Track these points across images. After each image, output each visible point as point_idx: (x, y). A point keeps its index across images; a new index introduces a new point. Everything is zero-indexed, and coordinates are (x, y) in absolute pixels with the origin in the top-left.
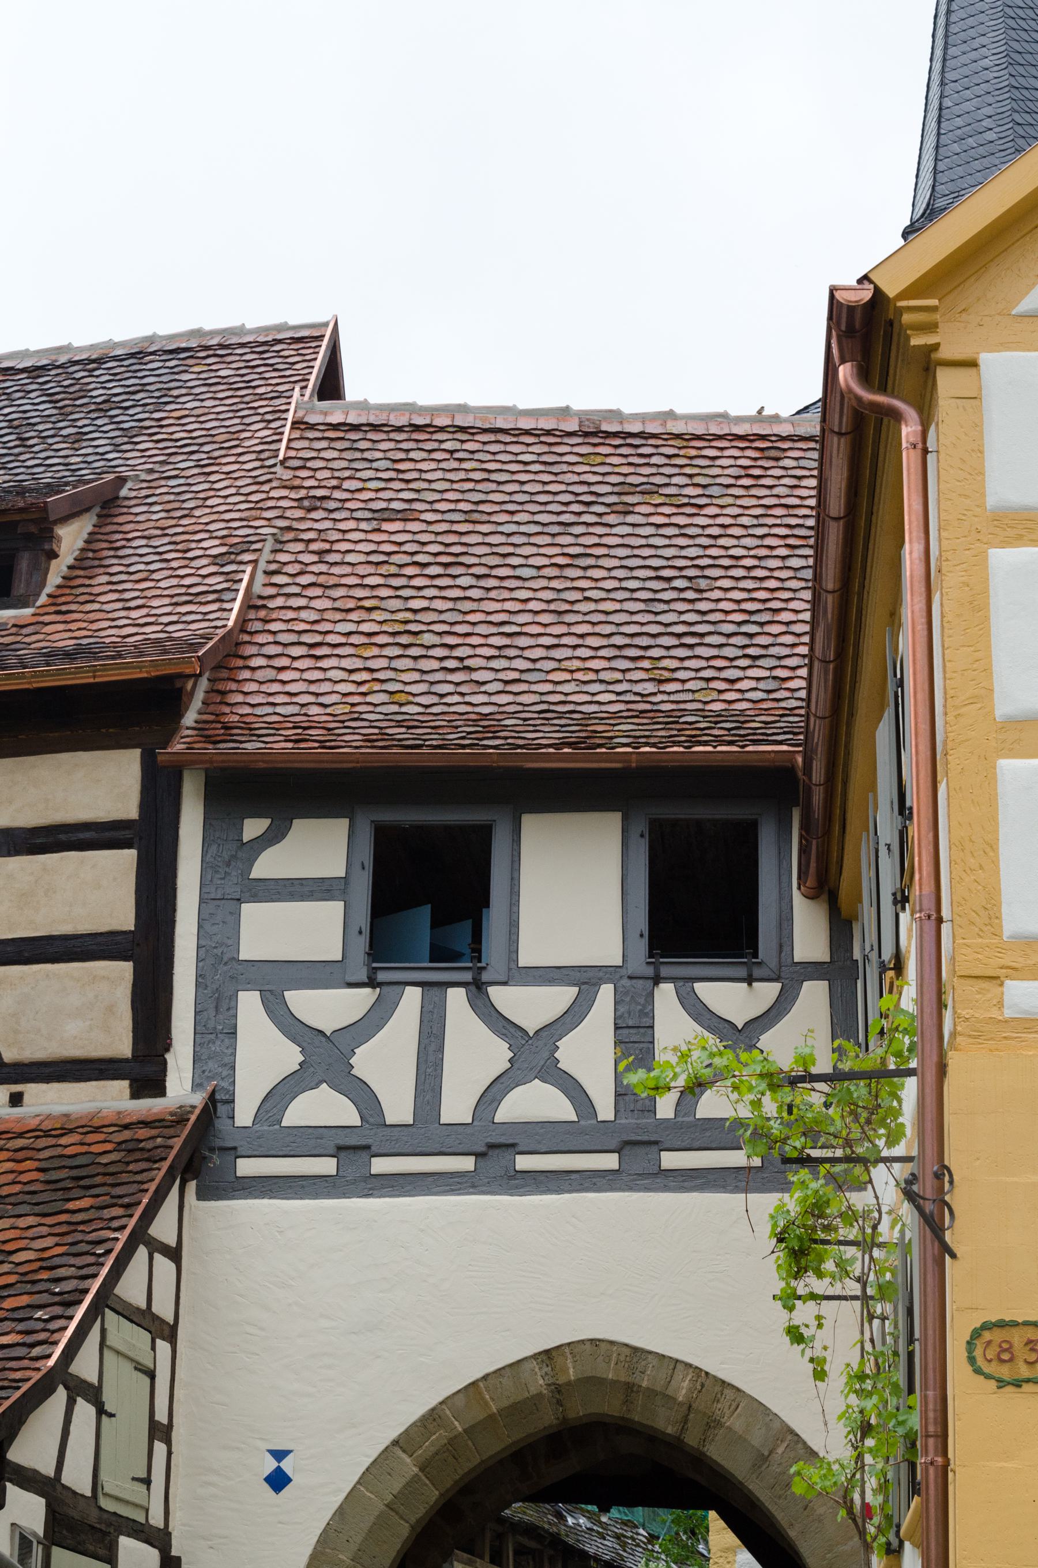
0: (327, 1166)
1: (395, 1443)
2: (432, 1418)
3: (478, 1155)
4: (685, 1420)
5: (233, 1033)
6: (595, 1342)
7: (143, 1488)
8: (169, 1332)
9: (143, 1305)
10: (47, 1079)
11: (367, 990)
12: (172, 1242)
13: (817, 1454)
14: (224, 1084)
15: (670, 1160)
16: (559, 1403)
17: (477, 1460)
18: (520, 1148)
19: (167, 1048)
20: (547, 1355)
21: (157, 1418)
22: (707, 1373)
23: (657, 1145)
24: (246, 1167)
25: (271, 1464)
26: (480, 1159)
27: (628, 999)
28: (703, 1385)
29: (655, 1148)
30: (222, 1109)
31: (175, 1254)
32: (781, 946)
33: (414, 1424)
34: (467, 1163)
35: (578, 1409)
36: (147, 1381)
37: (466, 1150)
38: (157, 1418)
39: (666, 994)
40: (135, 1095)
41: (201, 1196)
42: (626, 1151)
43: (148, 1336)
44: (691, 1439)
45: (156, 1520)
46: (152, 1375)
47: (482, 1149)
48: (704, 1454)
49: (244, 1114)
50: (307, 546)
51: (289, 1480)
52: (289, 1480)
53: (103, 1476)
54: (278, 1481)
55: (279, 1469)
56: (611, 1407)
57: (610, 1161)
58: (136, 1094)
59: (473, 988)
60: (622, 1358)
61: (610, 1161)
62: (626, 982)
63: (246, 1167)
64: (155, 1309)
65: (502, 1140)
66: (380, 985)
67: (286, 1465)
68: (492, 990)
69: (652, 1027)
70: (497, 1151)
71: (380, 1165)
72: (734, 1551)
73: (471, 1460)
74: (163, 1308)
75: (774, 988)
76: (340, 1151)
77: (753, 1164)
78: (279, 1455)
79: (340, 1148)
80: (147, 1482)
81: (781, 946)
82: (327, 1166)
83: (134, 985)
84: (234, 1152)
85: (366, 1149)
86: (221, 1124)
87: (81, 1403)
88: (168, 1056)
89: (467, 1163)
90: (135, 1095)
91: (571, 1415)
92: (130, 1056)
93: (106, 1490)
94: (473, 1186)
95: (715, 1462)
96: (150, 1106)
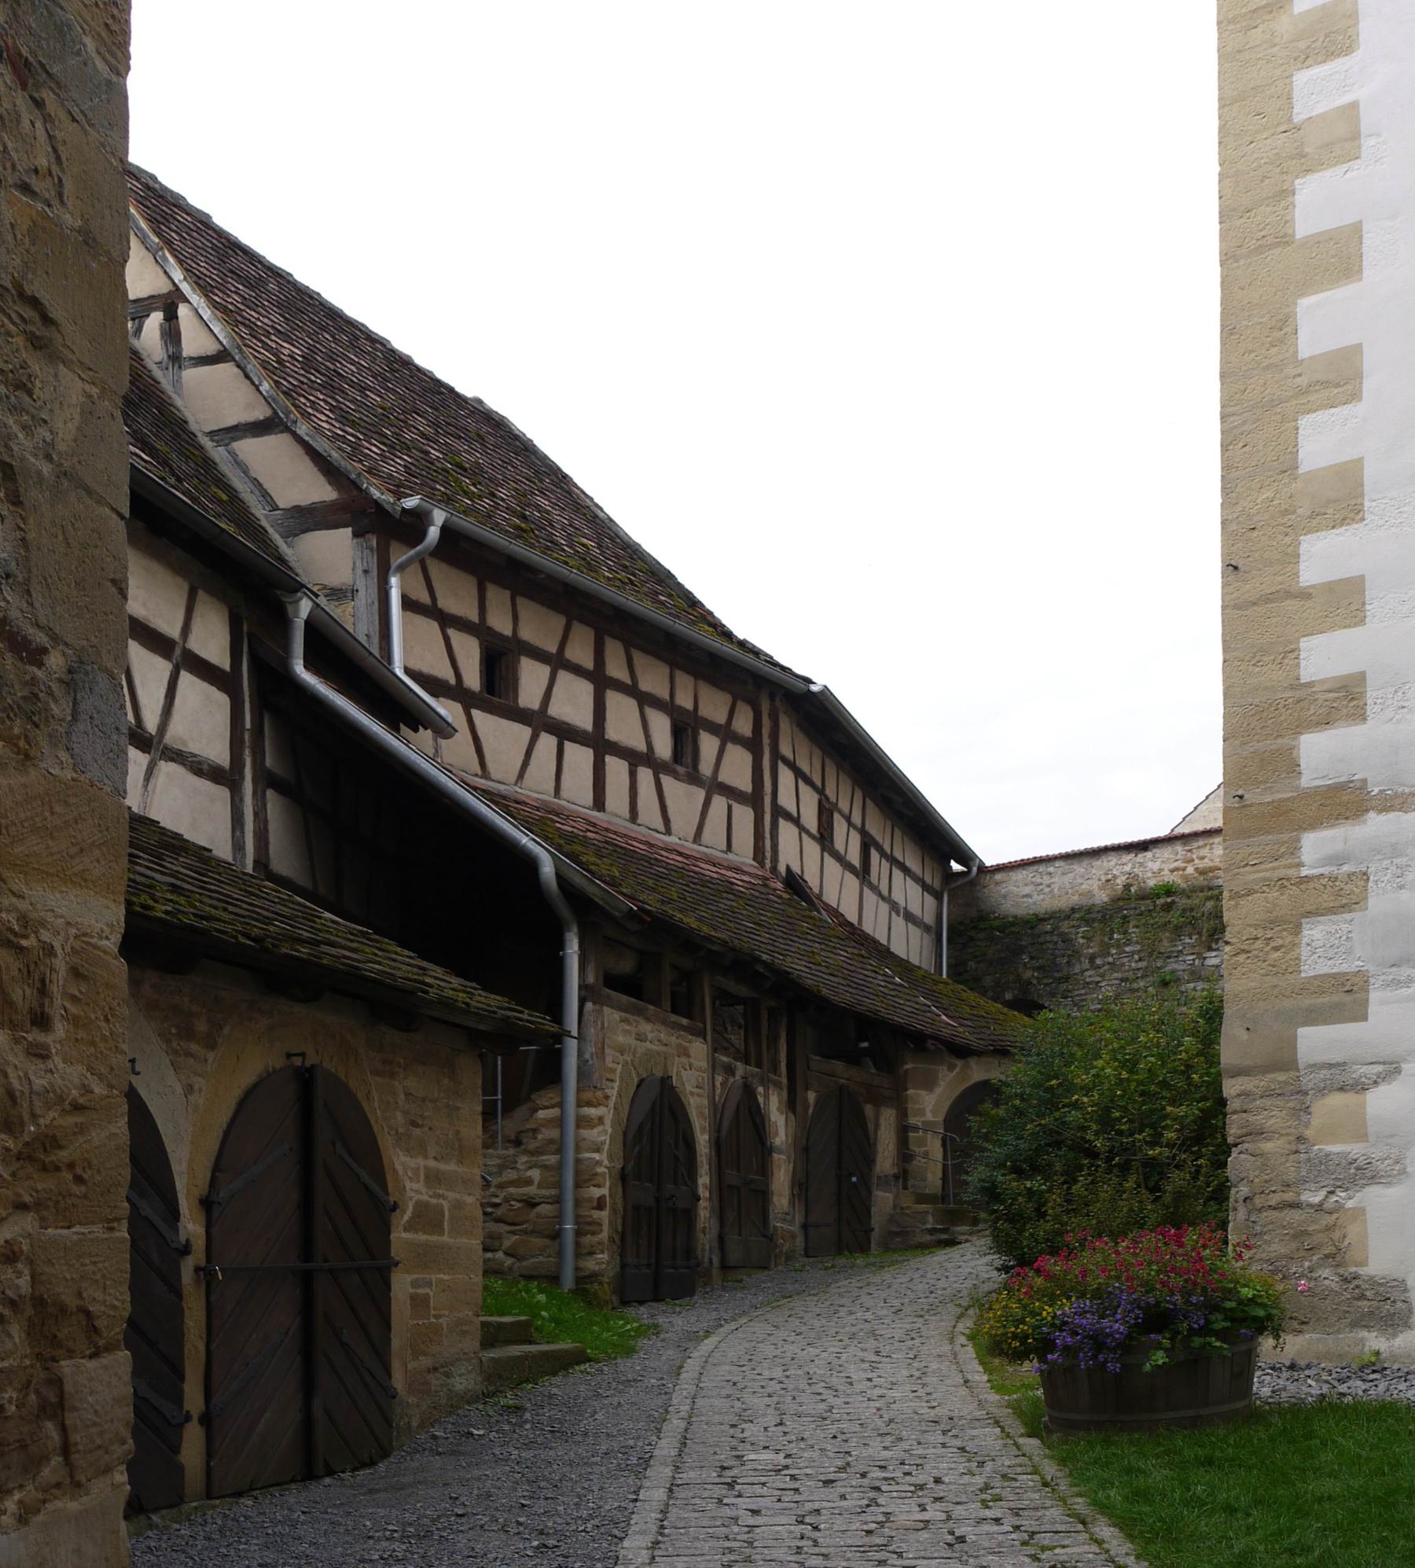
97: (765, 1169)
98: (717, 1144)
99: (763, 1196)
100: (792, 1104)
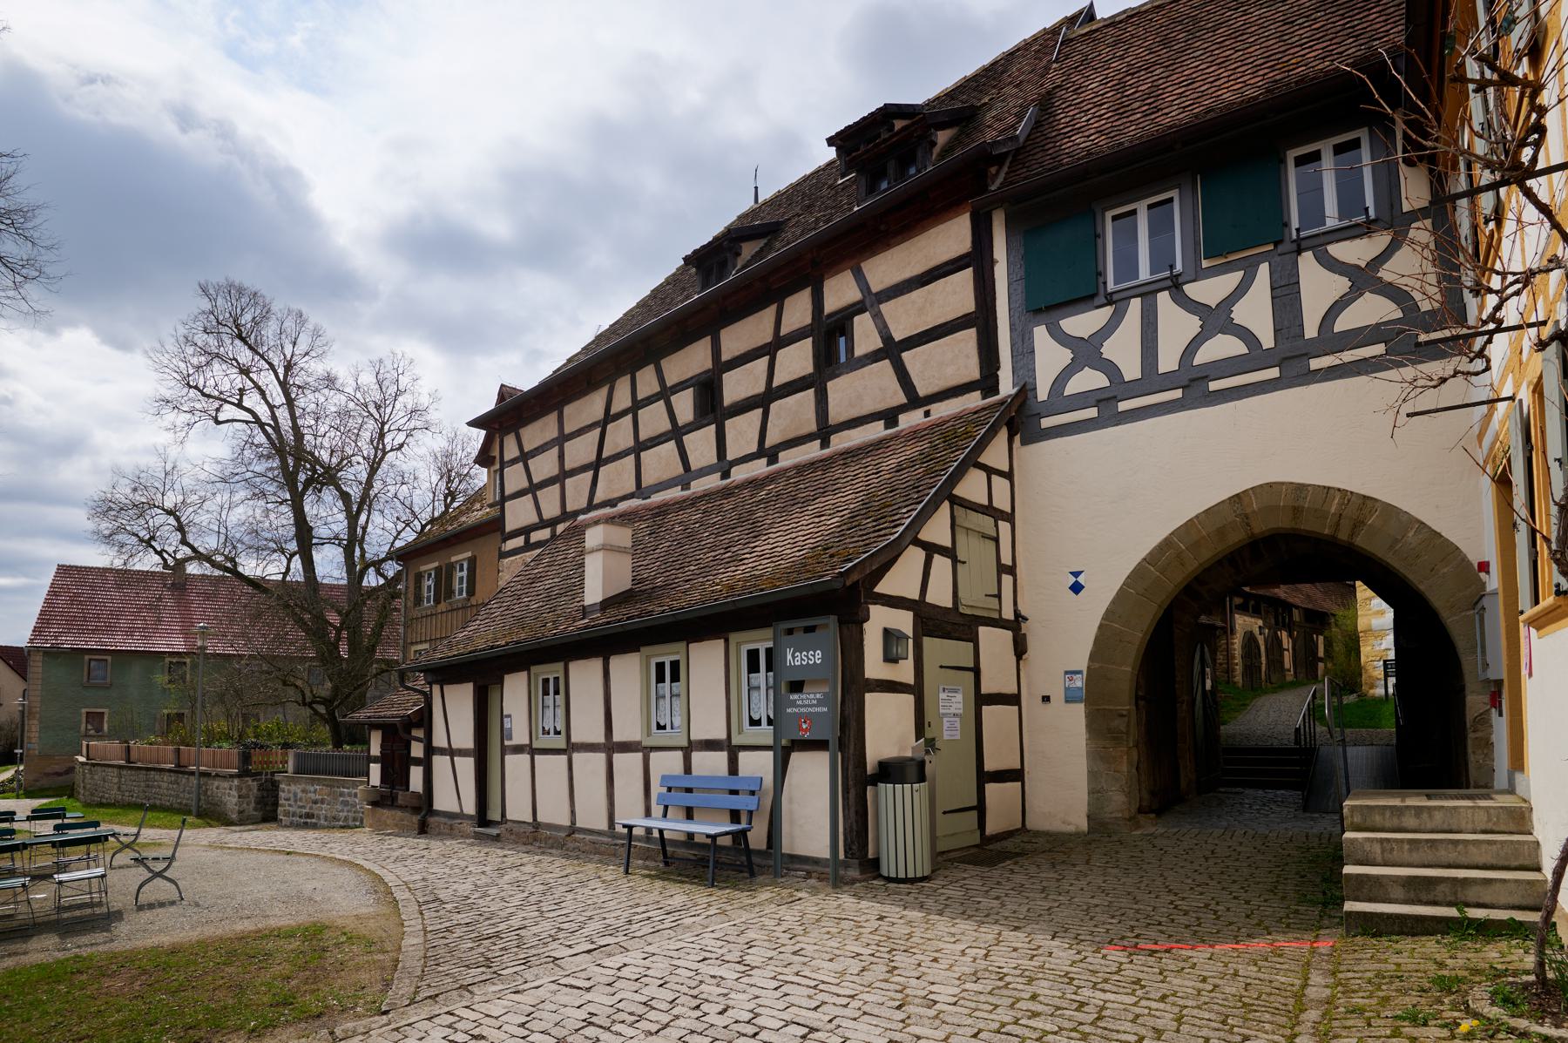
0: (1092, 412)
1: (1144, 559)
2: (1166, 544)
3: (1183, 387)
4: (1338, 524)
5: (1033, 352)
6: (1270, 485)
7: (996, 600)
8: (1010, 518)
9: (986, 503)
10: (941, 400)
11: (1108, 307)
12: (1006, 468)
13: (1439, 534)
14: (1031, 380)
15: (1315, 364)
16: (1248, 525)
17: (1196, 564)
18: (1119, 398)
19: (998, 368)
20: (1237, 498)
21: (1003, 562)
22: (1352, 493)
23: (1207, 378)
24: (1046, 423)
25: (1072, 580)
26: (1186, 390)
27: (1279, 269)
28: (1349, 501)
29: (1306, 358)
30: (1030, 394)
31: (1009, 475)
32: (1392, 205)
33: (1155, 548)
34: (1178, 394)
35: (1260, 527)
36: (992, 544)
37: (1175, 386)
38: (1003, 562)
39: (1040, 333)
40: (984, 398)
41: (1024, 443)
42: (1101, 404)
43: (992, 520)
44: (1343, 535)
45: (1008, 614)
46: (996, 540)
47: (1186, 383)
48: (1352, 544)
49: (1042, 394)
50: (527, 540)
51: (1083, 587)
52: (1083, 587)
53: (960, 594)
54: (1077, 588)
55: (1077, 582)
56: (1284, 522)
57: (1274, 373)
58: (887, 428)
59: (1173, 289)
60: (1289, 491)
61: (1274, 373)
62: (1278, 259)
63: (1046, 423)
64: (995, 504)
65: (1199, 375)
66: (1115, 302)
67: (1081, 579)
68: (1185, 287)
69: (1298, 283)
70: (1196, 382)
71: (1123, 406)
72: (1370, 599)
73: (1192, 565)
74: (1001, 502)
75: (1108, 311)
76: (1098, 403)
77: (391, 574)
78: (1076, 574)
79: (1099, 401)
80: (999, 596)
81: (1392, 205)
82: (1092, 412)
83: (978, 340)
84: (1040, 416)
85: (1116, 399)
86: (1030, 402)
87: (937, 558)
88: (999, 373)
89: (1178, 394)
90: (984, 398)
91: (1257, 531)
92: (906, 401)
93: (964, 602)
94: (1183, 406)
95: (1362, 549)
96: (826, 451)
97: (1282, 656)
98: (1266, 648)
99: (1282, 663)
100: (1290, 635)
